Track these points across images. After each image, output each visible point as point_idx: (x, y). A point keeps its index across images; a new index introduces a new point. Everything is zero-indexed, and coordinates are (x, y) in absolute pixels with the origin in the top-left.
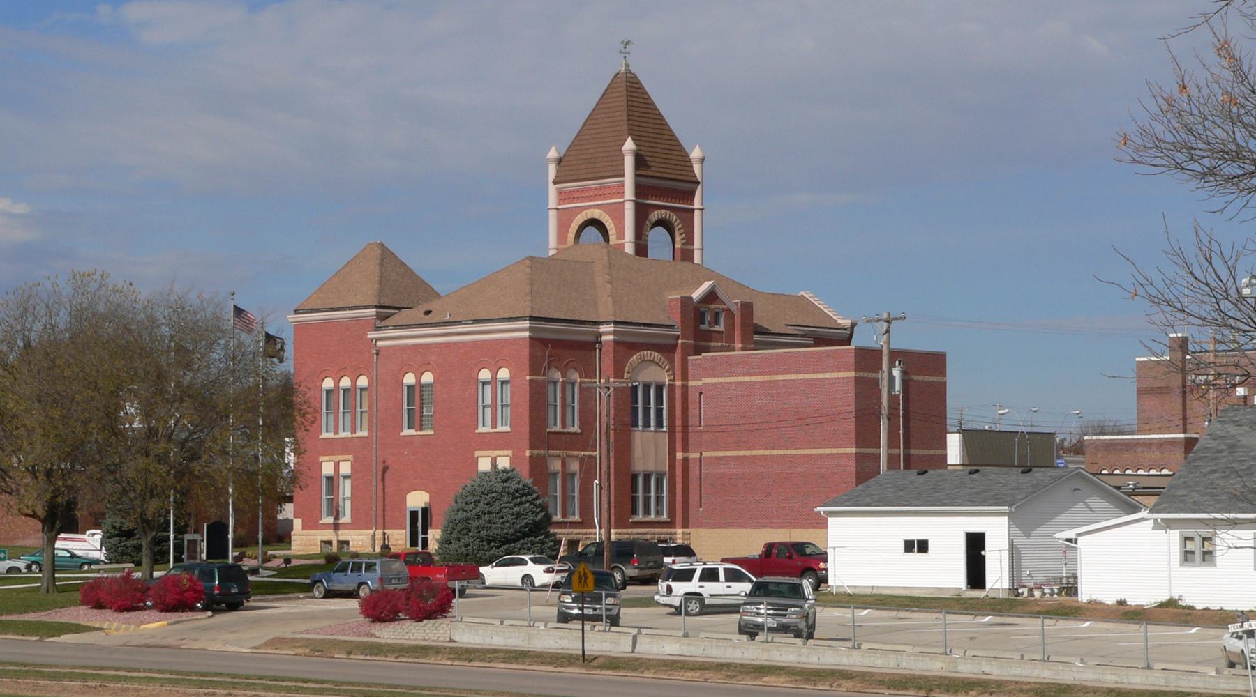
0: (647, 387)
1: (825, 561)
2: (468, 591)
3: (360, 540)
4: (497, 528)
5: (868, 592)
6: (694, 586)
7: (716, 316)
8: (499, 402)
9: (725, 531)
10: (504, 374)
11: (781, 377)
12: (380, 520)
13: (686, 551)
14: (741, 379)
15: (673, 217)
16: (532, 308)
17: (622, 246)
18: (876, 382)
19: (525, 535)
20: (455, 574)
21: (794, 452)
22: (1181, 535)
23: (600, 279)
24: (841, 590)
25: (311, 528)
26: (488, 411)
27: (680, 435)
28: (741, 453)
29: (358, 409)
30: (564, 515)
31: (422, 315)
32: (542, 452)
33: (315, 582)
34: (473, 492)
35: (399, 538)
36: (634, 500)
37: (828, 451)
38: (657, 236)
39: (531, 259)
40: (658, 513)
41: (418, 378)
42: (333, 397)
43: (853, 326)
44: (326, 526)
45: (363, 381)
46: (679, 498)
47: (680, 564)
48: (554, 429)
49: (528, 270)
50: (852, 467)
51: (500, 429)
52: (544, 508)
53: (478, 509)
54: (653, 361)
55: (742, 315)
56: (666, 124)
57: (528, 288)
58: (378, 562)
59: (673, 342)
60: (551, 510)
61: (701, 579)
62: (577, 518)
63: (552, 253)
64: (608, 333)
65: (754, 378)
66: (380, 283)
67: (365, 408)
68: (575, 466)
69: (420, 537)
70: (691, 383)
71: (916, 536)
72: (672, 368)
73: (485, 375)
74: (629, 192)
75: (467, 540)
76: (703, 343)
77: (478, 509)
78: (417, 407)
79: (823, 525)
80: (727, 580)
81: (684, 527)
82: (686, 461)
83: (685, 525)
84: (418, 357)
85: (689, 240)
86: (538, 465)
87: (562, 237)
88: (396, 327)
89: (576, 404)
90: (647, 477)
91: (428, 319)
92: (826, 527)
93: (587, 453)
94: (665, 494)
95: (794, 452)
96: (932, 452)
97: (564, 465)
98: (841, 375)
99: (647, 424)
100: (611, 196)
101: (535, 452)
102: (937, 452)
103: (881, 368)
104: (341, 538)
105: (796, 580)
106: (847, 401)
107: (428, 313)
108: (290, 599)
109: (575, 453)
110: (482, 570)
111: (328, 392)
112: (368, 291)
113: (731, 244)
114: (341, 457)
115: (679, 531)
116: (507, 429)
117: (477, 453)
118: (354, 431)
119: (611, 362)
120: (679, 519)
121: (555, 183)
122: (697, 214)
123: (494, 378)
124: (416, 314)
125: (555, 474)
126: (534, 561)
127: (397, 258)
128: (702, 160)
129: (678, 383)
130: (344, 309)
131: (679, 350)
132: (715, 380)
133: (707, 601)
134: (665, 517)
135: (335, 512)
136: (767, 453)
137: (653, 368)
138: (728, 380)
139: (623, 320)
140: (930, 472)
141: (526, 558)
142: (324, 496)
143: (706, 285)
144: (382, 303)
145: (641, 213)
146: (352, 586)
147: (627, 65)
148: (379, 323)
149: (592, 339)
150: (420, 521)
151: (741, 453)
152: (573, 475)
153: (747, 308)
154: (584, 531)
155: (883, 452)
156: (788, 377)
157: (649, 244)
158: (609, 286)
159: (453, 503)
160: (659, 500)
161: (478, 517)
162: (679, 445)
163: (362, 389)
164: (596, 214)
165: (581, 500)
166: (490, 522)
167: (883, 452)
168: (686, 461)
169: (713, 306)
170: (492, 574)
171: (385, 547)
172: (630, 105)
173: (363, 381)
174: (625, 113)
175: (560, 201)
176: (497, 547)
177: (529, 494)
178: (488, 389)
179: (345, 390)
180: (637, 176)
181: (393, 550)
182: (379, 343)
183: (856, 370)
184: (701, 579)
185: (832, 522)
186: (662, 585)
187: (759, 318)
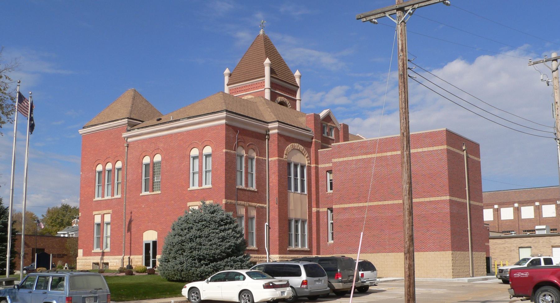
4: (206, 249)
10: (208, 150)
11: (389, 154)
19: (228, 255)
22: (552, 264)
26: (196, 176)
27: (315, 198)
29: (116, 181)
32: (233, 201)
35: (138, 261)
40: (303, 245)
41: (152, 159)
42: (102, 175)
44: (96, 254)
45: (119, 165)
48: (240, 187)
53: (191, 234)
54: (299, 150)
59: (309, 140)
64: (274, 129)
66: (132, 107)
67: (120, 181)
68: (253, 213)
69: (151, 260)
70: (320, 166)
72: (309, 156)
73: (195, 152)
74: (267, 84)
75: (182, 259)
77: (191, 234)
78: (150, 177)
82: (318, 213)
84: (152, 146)
89: (254, 172)
93: (261, 205)
94: (306, 233)
99: (296, 189)
101: (229, 201)
114: (105, 212)
118: (113, 195)
119: (276, 147)
121: (228, 85)
123: (201, 153)
125: (241, 218)
126: (250, 274)
129: (313, 165)
131: (313, 145)
134: (306, 248)
137: (299, 155)
141: (243, 272)
142: (95, 236)
144: (132, 117)
150: (150, 250)
152: (252, 218)
154: (259, 256)
159: (171, 231)
161: (191, 240)
162: (314, 203)
165: (257, 235)
166: (200, 244)
168: (318, 213)
169: (329, 124)
171: (130, 267)
173: (119, 165)
176: (207, 265)
177: (230, 223)
180: (271, 77)
183: (448, 144)
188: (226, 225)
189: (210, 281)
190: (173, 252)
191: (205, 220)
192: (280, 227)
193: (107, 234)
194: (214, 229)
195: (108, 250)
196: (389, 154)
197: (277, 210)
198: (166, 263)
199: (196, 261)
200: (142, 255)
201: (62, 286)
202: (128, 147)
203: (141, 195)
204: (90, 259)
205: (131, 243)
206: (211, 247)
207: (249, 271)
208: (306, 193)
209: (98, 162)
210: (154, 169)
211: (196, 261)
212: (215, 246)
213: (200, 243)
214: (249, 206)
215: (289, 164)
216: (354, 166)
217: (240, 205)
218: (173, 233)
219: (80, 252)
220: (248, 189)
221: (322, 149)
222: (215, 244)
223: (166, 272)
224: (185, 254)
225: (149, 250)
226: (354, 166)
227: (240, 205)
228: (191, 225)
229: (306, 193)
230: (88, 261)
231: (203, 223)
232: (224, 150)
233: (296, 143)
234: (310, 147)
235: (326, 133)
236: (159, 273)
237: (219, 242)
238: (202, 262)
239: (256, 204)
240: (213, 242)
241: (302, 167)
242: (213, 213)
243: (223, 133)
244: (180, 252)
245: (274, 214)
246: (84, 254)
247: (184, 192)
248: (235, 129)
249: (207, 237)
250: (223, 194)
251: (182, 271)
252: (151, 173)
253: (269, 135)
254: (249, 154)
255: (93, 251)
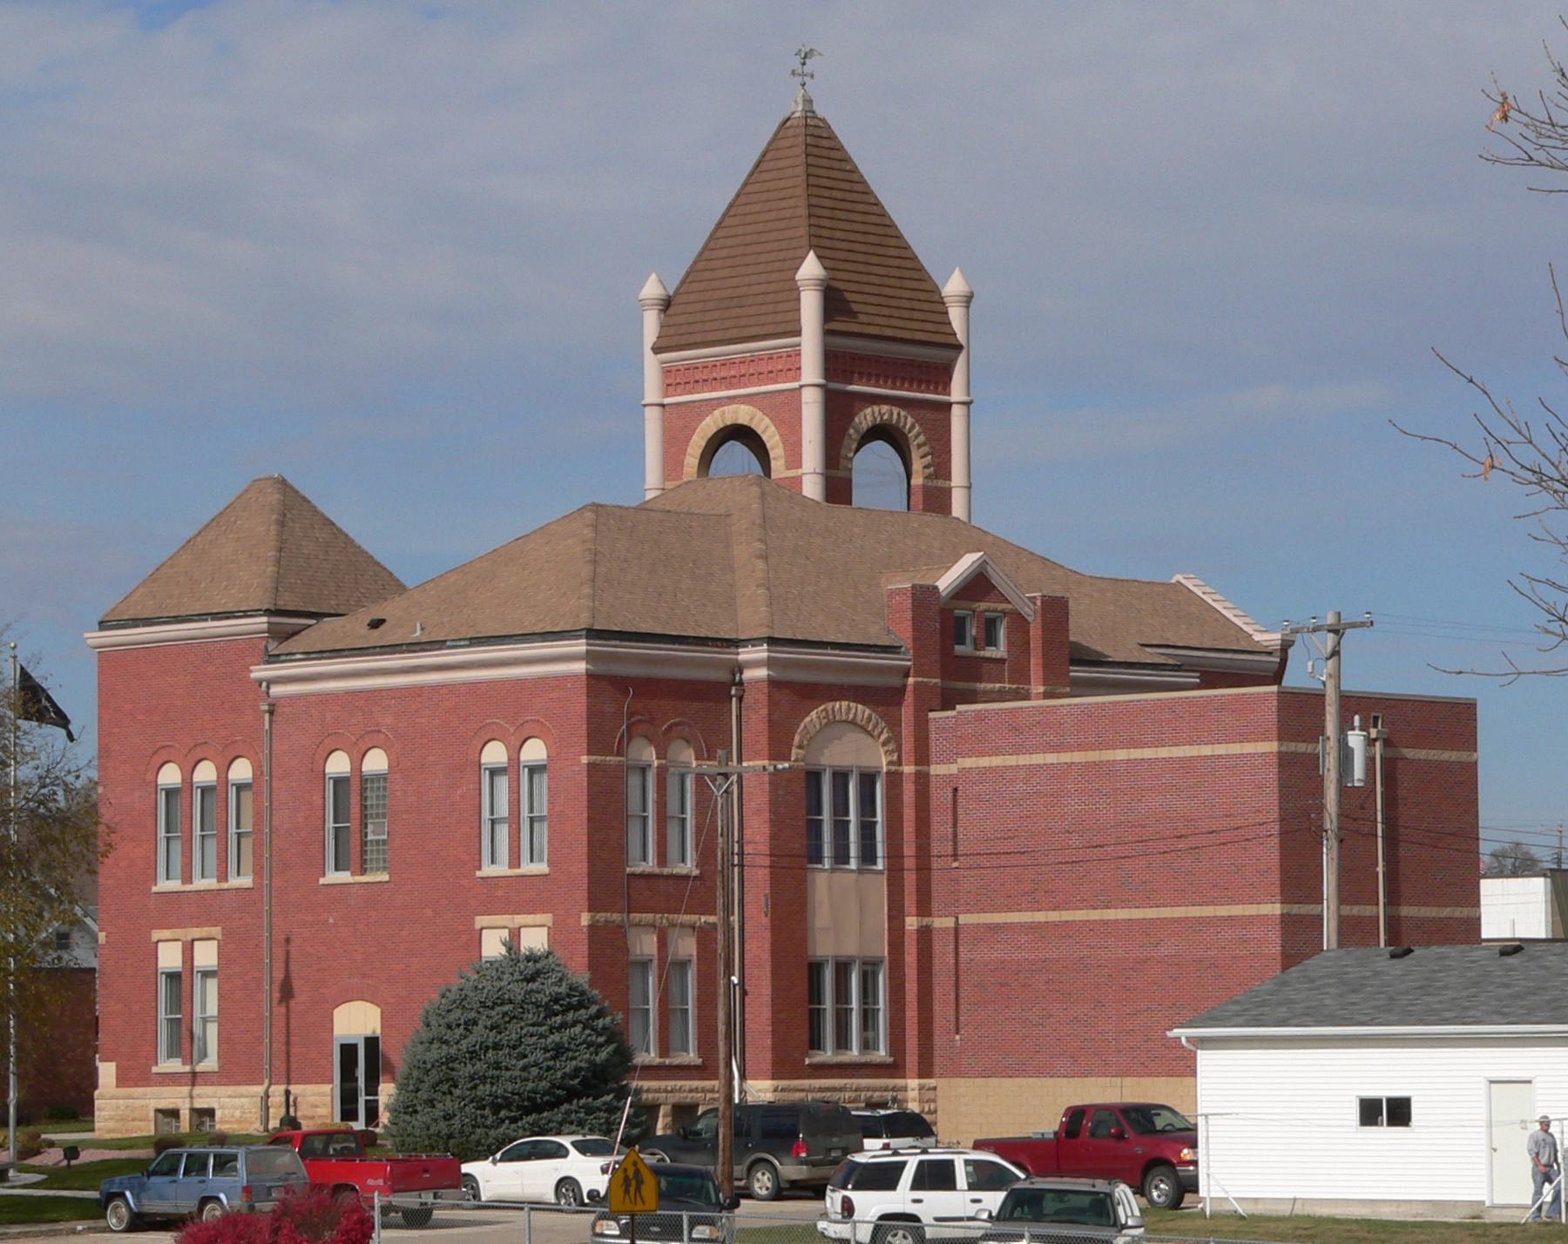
0: (841, 778)
1: (1193, 1145)
2: (437, 1214)
3: (238, 1108)
4: (512, 1080)
5: (1285, 1210)
6: (900, 1199)
7: (990, 627)
8: (525, 813)
9: (1008, 1081)
10: (535, 751)
11: (1121, 755)
12: (280, 1065)
13: (916, 1126)
14: (1038, 759)
15: (907, 421)
16: (594, 612)
17: (798, 481)
18: (1313, 762)
19: (572, 1094)
20: (406, 1176)
21: (1151, 913)
23: (744, 551)
24: (1226, 1207)
25: (136, 1083)
26: (503, 832)
27: (914, 881)
28: (1040, 917)
29: (232, 829)
30: (664, 1050)
31: (364, 630)
32: (616, 917)
33: (111, 1197)
34: (461, 1003)
35: (318, 1103)
36: (815, 1018)
37: (1222, 911)
38: (874, 466)
39: (597, 508)
40: (867, 1045)
42: (180, 803)
43: (1285, 646)
44: (171, 1079)
45: (241, 771)
46: (911, 1013)
47: (873, 1150)
49: (588, 533)
50: (1273, 945)
51: (527, 868)
52: (615, 1036)
53: (472, 1039)
54: (853, 722)
55: (1045, 627)
56: (892, 226)
57: (586, 571)
58: (241, 1152)
59: (895, 681)
60: (634, 1039)
61: (918, 1184)
62: (692, 1057)
63: (650, 495)
64: (755, 664)
65: (1066, 757)
67: (247, 827)
68: (687, 947)
69: (362, 1099)
70: (935, 769)
71: (1384, 1090)
72: (896, 738)
73: (495, 754)
74: (811, 368)
75: (449, 1105)
76: (960, 685)
77: (472, 1039)
78: (354, 825)
79: (1188, 1069)
80: (972, 1187)
81: (920, 1076)
82: (925, 934)
83: (925, 1071)
84: (357, 719)
85: (941, 468)
86: (607, 948)
87: (672, 464)
88: (309, 655)
90: (842, 969)
91: (376, 637)
92: (1192, 1072)
95: (1151, 913)
96: (1446, 912)
97: (663, 944)
98: (1248, 748)
99: (841, 857)
100: (772, 376)
101: (602, 917)
102: (1460, 912)
103: (1321, 730)
104: (199, 1104)
105: (1101, 1185)
106: (1263, 802)
107: (376, 624)
108: (55, 1233)
109: (687, 918)
110: (466, 1168)
111: (170, 793)
112: (252, 579)
113: (1032, 480)
114: (196, 932)
115: (913, 1083)
116: (541, 868)
117: (480, 921)
118: (223, 877)
119: (763, 727)
120: (912, 1059)
121: (657, 350)
122: (957, 413)
123: (514, 760)
124: (352, 628)
125: (644, 965)
126: (583, 1148)
127: (314, 510)
128: (968, 300)
129: (908, 769)
130: (202, 617)
131: (909, 698)
132: (985, 762)
133: (929, 1233)
134: (882, 1054)
135: (184, 1041)
136: (1095, 915)
138: (1011, 760)
139: (789, 636)
140: (1418, 952)
141: (566, 1141)
142: (162, 1015)
143: (966, 563)
145: (837, 410)
146: (186, 1205)
147: (808, 101)
148: (273, 647)
149: (722, 675)
150: (361, 1065)
151: (1040, 917)
153: (1055, 610)
155: (1329, 910)
156: (1136, 754)
157: (856, 478)
158: (760, 564)
159: (420, 1026)
160: (868, 1018)
161: (473, 1055)
162: (910, 901)
163: (240, 788)
164: (743, 414)
167: (1329, 910)
168: (925, 934)
169: (982, 606)
170: (495, 1177)
171: (291, 1122)
172: (812, 185)
173: (241, 771)
174: (802, 202)
175: (669, 387)
176: (514, 1120)
177: (581, 1005)
178: (503, 783)
179: (206, 790)
180: (827, 333)
181: (306, 1126)
182: (276, 690)
183: (1280, 739)
184: (918, 1184)
185: (1206, 1060)
186: (834, 1199)
187: (1082, 630)
188: (564, 1012)
189: (501, 1160)
190: (425, 1086)
191: (511, 1002)
192: (776, 989)
193: (204, 1009)
194: (533, 1025)
195: (211, 1063)
196: (1121, 755)
197: (767, 934)
198: (407, 1117)
199: (487, 1111)
200: (331, 1081)
201: (235, 1169)
202: (271, 713)
203: (322, 881)
204: (144, 1097)
205: (288, 1043)
206: (524, 1074)
207: (580, 1138)
208: (880, 865)
209: (164, 755)
210: (363, 798)
211: (487, 1111)
212: (535, 1071)
213: (497, 1063)
214: (673, 925)
215: (814, 777)
216: (1020, 786)
217: (638, 925)
218: (425, 1035)
219: (107, 1072)
220: (666, 871)
221: (943, 709)
222: (536, 1064)
223: (408, 1140)
224: (457, 1092)
225: (356, 1065)
226: (1020, 786)
227: (638, 925)
228: (473, 1015)
229: (880, 865)
230: (143, 1102)
231: (506, 1008)
232: (584, 759)
233: (841, 699)
234: (899, 704)
235: (968, 640)
236: (389, 1144)
237: (546, 1060)
238: (503, 1113)
239: (694, 918)
240: (531, 1059)
241: (868, 780)
242: (531, 979)
243: (580, 703)
244: (445, 1087)
245: (759, 948)
246: (123, 1080)
247: (465, 882)
248: (620, 684)
249: (514, 1048)
250: (582, 895)
251: (450, 1136)
252: (355, 810)
253: (741, 683)
254: (670, 755)
255: (155, 1069)
